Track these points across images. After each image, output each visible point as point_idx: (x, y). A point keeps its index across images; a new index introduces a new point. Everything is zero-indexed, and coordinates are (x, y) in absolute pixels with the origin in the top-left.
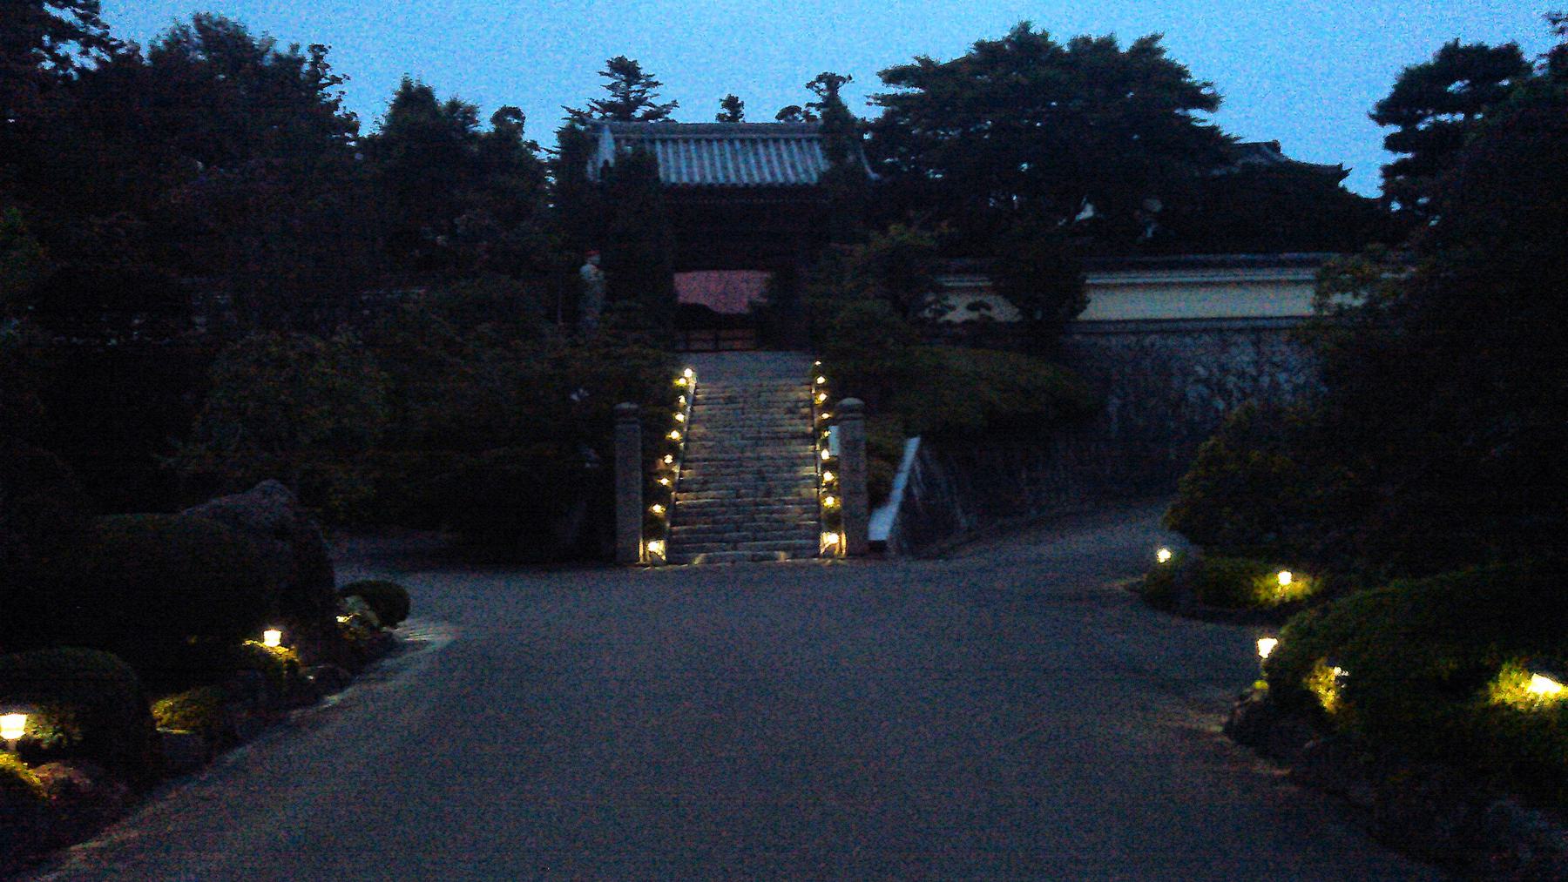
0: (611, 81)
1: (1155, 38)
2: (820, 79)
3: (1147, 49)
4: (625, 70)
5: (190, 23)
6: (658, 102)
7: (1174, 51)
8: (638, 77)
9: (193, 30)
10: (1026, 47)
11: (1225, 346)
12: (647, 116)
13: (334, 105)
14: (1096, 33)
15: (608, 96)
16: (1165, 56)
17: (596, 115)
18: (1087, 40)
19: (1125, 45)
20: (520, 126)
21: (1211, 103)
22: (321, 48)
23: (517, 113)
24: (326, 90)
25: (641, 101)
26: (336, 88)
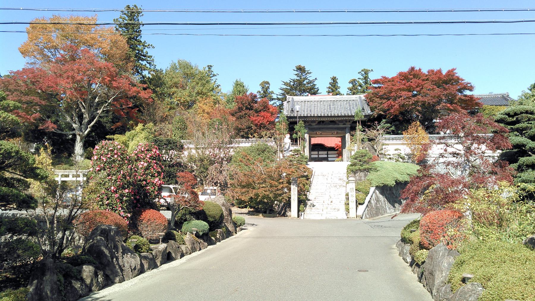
0: (297, 73)
1: (454, 70)
2: (362, 71)
3: (451, 73)
4: (301, 69)
5: (177, 62)
6: (311, 79)
7: (460, 73)
8: (305, 71)
9: (177, 64)
10: (413, 74)
11: (62, 290)
12: (308, 83)
13: (127, 254)
14: (436, 68)
15: (296, 78)
16: (457, 75)
17: (292, 84)
18: (433, 71)
19: (444, 72)
20: (268, 87)
21: (471, 89)
22: (211, 66)
23: (268, 83)
24: (212, 78)
25: (306, 79)
26: (215, 77)
